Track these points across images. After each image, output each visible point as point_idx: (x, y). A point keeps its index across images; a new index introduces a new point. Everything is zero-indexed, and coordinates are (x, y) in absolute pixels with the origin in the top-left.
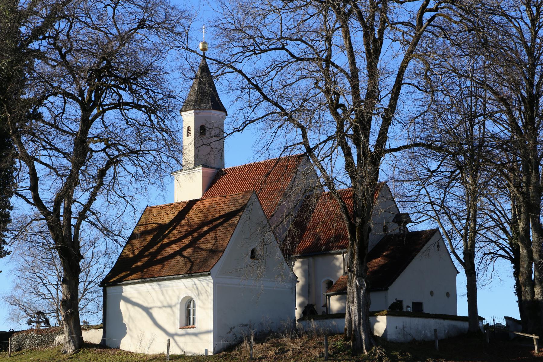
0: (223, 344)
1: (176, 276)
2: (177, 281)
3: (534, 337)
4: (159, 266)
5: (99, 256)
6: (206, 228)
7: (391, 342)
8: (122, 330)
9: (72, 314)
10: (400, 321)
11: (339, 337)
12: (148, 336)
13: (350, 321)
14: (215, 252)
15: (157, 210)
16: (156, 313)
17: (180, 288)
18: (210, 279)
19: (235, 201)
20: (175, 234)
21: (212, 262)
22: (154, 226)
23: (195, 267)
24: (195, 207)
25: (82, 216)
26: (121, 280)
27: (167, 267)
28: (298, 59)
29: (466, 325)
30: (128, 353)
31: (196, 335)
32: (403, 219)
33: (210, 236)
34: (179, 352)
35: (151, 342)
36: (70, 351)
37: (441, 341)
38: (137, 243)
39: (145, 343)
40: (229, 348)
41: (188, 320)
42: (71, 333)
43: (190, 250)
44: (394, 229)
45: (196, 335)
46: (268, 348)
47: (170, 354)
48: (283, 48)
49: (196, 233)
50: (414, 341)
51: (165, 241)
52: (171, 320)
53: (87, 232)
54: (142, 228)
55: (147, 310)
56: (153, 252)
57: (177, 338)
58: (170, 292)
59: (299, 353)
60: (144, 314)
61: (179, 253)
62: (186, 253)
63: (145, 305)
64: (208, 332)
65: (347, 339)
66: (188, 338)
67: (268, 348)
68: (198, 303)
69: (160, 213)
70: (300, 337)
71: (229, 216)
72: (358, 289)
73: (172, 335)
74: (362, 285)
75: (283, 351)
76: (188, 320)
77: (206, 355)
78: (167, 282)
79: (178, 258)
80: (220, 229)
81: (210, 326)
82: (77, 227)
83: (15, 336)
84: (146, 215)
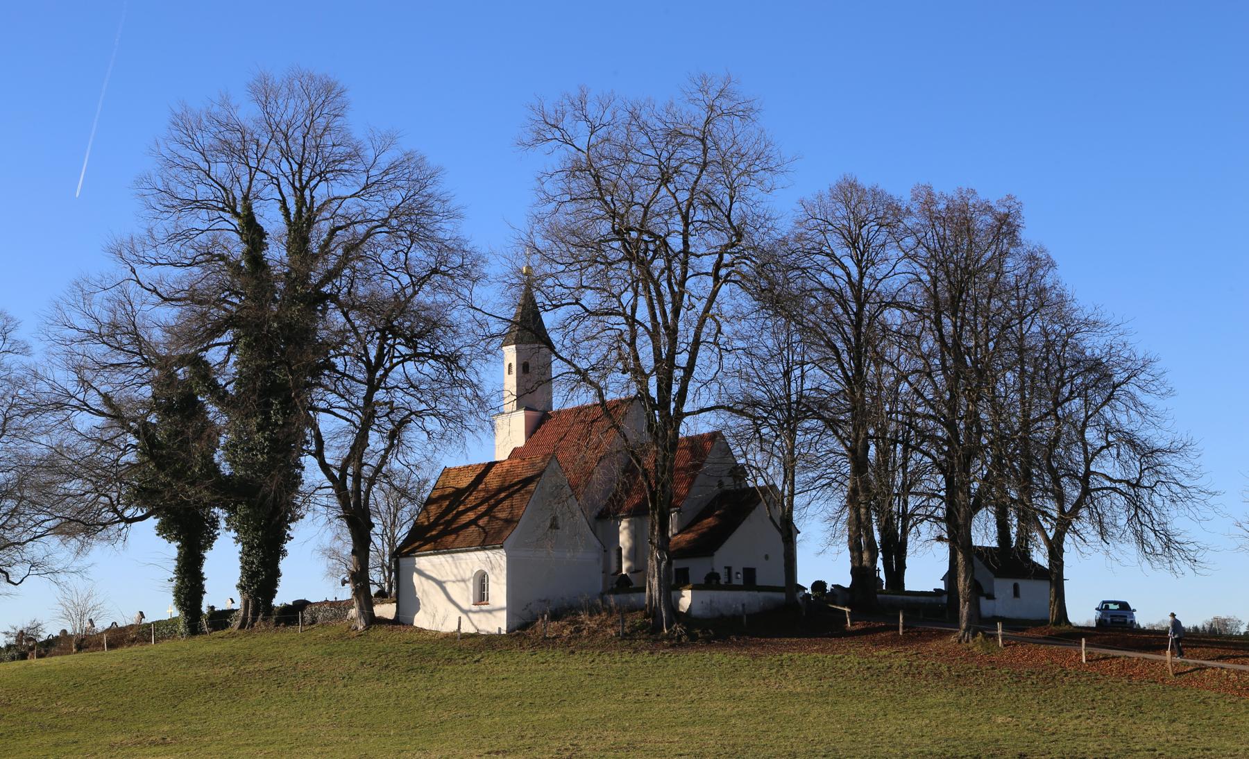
0: (517, 622)
1: (468, 548)
2: (471, 554)
3: (847, 610)
4: (453, 536)
5: (390, 525)
6: (503, 495)
7: (696, 618)
8: (416, 605)
9: (362, 587)
10: (707, 595)
11: (639, 614)
12: (441, 613)
13: (651, 597)
14: (510, 522)
15: (455, 472)
16: (449, 587)
17: (474, 561)
18: (502, 552)
19: (533, 464)
20: (472, 500)
21: (506, 533)
22: (450, 490)
23: (489, 539)
24: (493, 470)
25: (372, 482)
26: (414, 551)
27: (461, 538)
28: (591, 313)
29: (781, 596)
30: (421, 630)
31: (490, 612)
32: (739, 472)
33: (507, 503)
34: (472, 630)
35: (445, 618)
36: (361, 627)
37: (748, 616)
38: (433, 509)
39: (439, 618)
40: (524, 626)
41: (482, 596)
42: (361, 608)
43: (486, 519)
44: (729, 483)
45: (490, 612)
46: (564, 627)
47: (463, 631)
48: (577, 303)
49: (493, 499)
50: (722, 616)
51: (461, 508)
52: (464, 595)
53: (378, 497)
54: (437, 493)
55: (440, 584)
56: (450, 518)
57: (471, 615)
58: (464, 566)
59: (595, 631)
60: (438, 587)
61: (474, 522)
62: (481, 523)
63: (439, 578)
64: (501, 609)
65: (647, 616)
66: (482, 615)
67: (564, 627)
68: (492, 578)
69: (458, 475)
70: (599, 614)
71: (527, 481)
72: (659, 563)
73: (466, 612)
74: (663, 558)
75: (578, 630)
76: (482, 596)
77: (500, 634)
78: (461, 555)
79: (473, 528)
80: (517, 496)
81: (504, 603)
82: (367, 493)
83: (308, 608)
84: (443, 478)
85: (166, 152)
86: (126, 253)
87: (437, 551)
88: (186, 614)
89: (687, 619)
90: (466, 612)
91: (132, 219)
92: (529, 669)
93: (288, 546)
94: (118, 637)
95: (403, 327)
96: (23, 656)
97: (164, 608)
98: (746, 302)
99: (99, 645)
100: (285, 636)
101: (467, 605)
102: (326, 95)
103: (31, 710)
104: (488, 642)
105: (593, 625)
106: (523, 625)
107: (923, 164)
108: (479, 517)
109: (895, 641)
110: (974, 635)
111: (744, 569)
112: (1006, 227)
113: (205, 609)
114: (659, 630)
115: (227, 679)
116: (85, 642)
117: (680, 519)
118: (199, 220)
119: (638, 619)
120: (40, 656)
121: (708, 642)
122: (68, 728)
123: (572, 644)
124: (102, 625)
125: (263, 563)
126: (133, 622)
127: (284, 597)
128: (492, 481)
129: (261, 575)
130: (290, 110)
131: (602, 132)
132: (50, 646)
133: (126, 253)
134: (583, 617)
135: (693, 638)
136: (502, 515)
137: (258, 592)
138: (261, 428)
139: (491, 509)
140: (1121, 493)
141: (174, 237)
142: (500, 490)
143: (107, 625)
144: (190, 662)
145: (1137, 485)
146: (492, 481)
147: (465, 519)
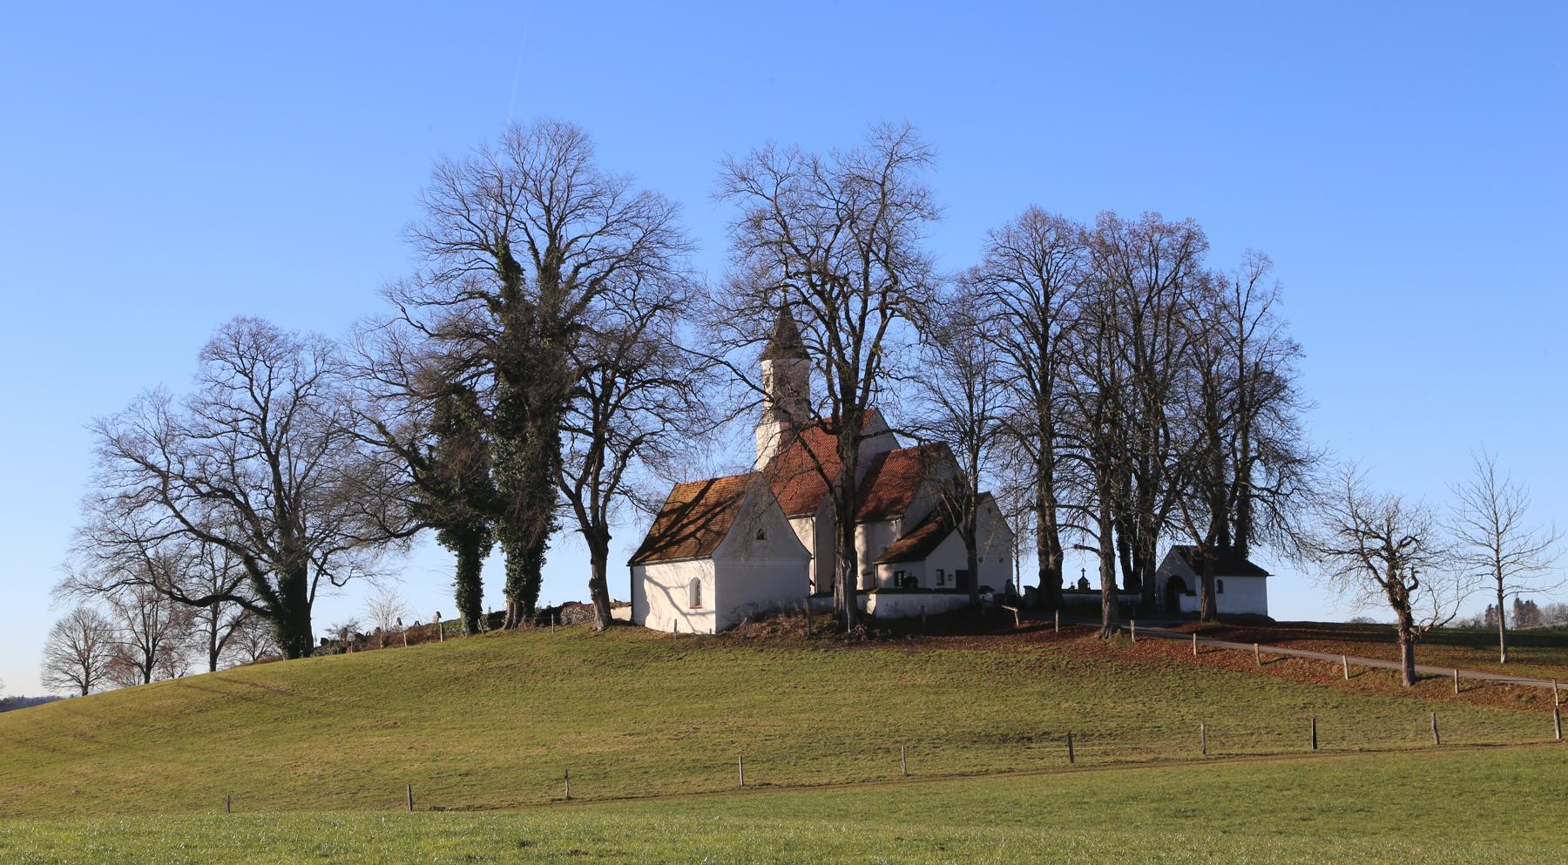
0: (725, 624)
11: (829, 616)
16: (672, 592)
20: (693, 514)
33: (720, 517)
34: (690, 631)
39: (664, 620)
40: (730, 628)
41: (697, 603)
49: (711, 512)
52: (683, 599)
55: (665, 589)
61: (693, 534)
68: (703, 585)
72: (844, 570)
75: (774, 631)
79: (692, 540)
85: (430, 200)
86: (398, 295)
87: (662, 560)
88: (467, 614)
89: (872, 621)
90: (685, 615)
91: (407, 263)
92: (727, 663)
93: (547, 555)
94: (419, 634)
95: (630, 358)
96: (343, 651)
97: (452, 613)
98: (912, 334)
99: (400, 641)
100: (539, 636)
101: (686, 608)
102: (568, 142)
103: (307, 699)
104: (698, 642)
105: (787, 625)
106: (729, 631)
107: (1103, 191)
108: (697, 530)
109: (1051, 638)
110: (1114, 632)
111: (958, 572)
112: (1188, 246)
113: (485, 612)
114: (843, 627)
115: (470, 674)
116: (388, 639)
117: (904, 525)
118: (458, 260)
119: (827, 620)
120: (356, 650)
121: (884, 641)
122: (330, 714)
123: (762, 644)
124: (408, 623)
125: (524, 570)
126: (431, 621)
127: (542, 602)
128: (711, 497)
129: (525, 581)
130: (539, 158)
131: (785, 184)
132: (363, 642)
133: (398, 295)
134: (781, 618)
135: (871, 636)
136: (715, 528)
137: (520, 596)
138: (519, 449)
139: (707, 522)
140: (1263, 500)
141: (440, 278)
142: (717, 504)
143: (411, 624)
144: (447, 659)
145: (1274, 493)
146: (711, 497)
147: (687, 531)
